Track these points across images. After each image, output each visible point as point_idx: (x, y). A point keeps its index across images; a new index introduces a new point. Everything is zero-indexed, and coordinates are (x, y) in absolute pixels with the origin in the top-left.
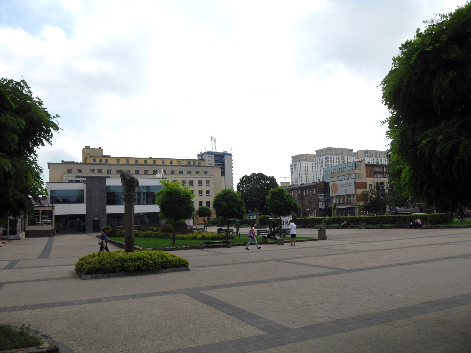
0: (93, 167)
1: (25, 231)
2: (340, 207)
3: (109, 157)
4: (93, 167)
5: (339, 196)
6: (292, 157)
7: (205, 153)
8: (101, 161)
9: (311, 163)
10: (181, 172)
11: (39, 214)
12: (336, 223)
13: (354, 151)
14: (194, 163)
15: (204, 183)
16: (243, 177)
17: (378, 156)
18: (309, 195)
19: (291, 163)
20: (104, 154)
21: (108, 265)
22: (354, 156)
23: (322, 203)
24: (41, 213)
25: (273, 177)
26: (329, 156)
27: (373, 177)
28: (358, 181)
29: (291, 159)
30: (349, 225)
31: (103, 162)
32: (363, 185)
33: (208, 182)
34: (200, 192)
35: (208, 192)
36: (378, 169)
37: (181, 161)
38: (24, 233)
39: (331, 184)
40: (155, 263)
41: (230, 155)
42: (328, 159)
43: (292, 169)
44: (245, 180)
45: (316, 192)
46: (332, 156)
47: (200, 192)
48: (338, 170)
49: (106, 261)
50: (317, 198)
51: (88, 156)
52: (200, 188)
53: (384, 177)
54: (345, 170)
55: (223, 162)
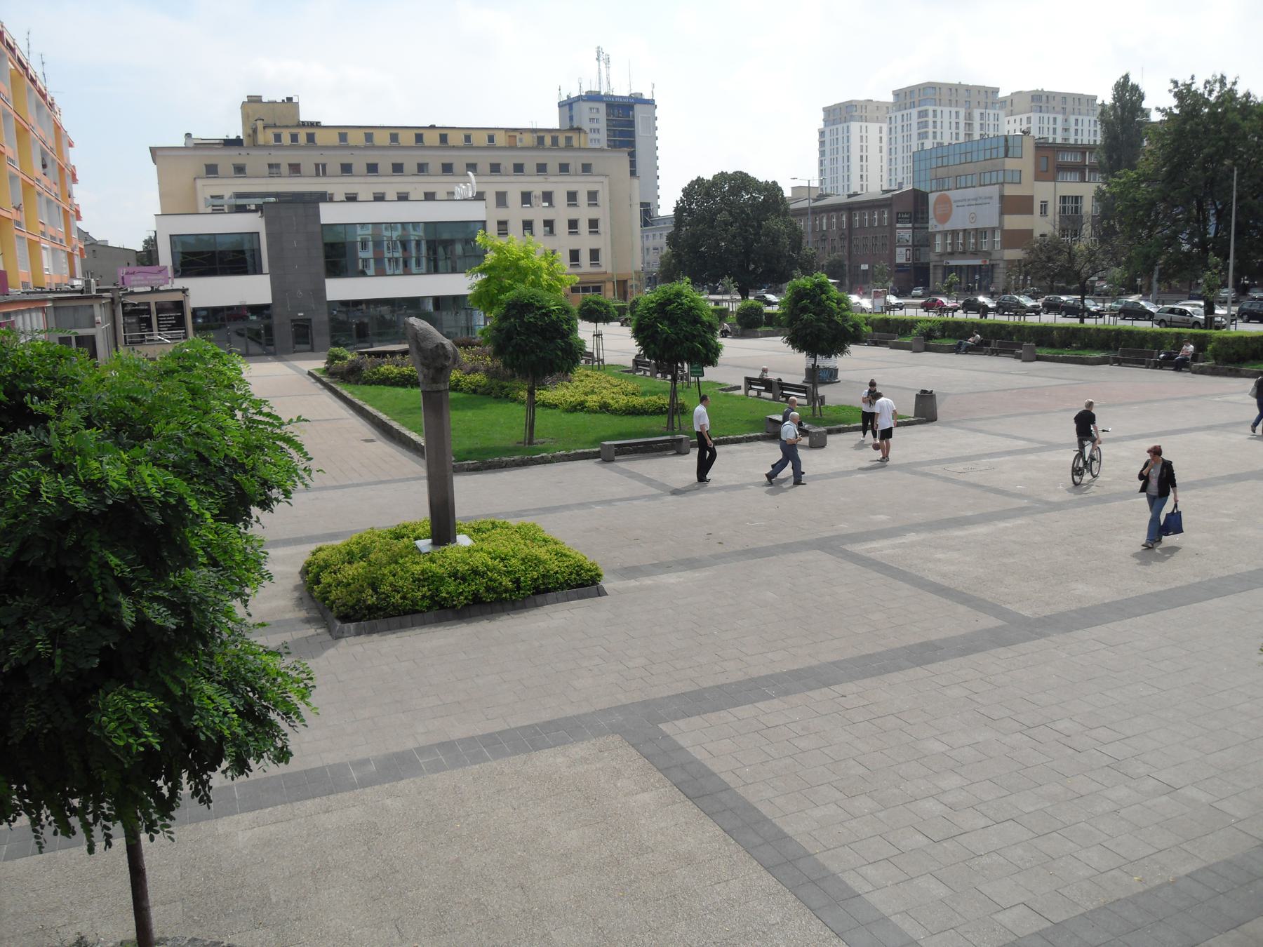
2: (953, 263)
3: (316, 125)
5: (954, 233)
6: (824, 109)
7: (579, 98)
8: (294, 138)
9: (877, 125)
10: (519, 168)
11: (148, 311)
12: (950, 337)
13: (1001, 95)
14: (555, 141)
15: (583, 198)
16: (692, 184)
17: (1069, 109)
18: (871, 225)
19: (821, 125)
20: (302, 119)
21: (398, 597)
22: (1001, 108)
23: (904, 250)
24: (153, 308)
25: (775, 183)
26: (931, 109)
27: (1054, 180)
28: (1010, 191)
29: (821, 115)
30: (988, 344)
31: (302, 139)
32: (1022, 205)
33: (593, 196)
34: (573, 224)
35: (593, 224)
36: (1069, 158)
39: (932, 198)
40: (517, 581)
41: (651, 103)
42: (926, 115)
43: (822, 143)
44: (696, 190)
45: (890, 218)
46: (939, 109)
47: (573, 224)
48: (957, 158)
49: (391, 584)
50: (893, 234)
51: (260, 124)
52: (573, 213)
53: (1083, 180)
54: (975, 159)
55: (631, 124)
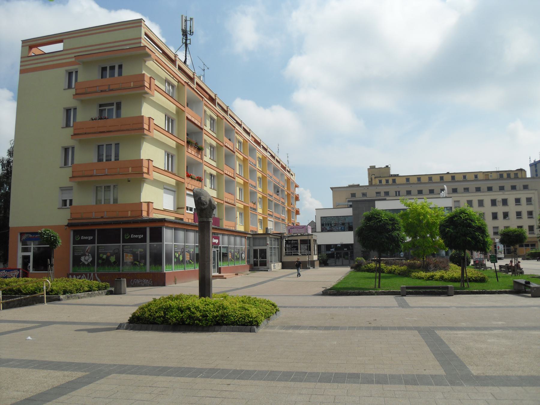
0: (379, 189)
1: (281, 261)
3: (397, 175)
4: (379, 189)
8: (387, 181)
11: (297, 243)
15: (523, 201)
24: (299, 242)
31: (390, 181)
33: (529, 200)
35: (530, 213)
37: (490, 174)
38: (280, 264)
